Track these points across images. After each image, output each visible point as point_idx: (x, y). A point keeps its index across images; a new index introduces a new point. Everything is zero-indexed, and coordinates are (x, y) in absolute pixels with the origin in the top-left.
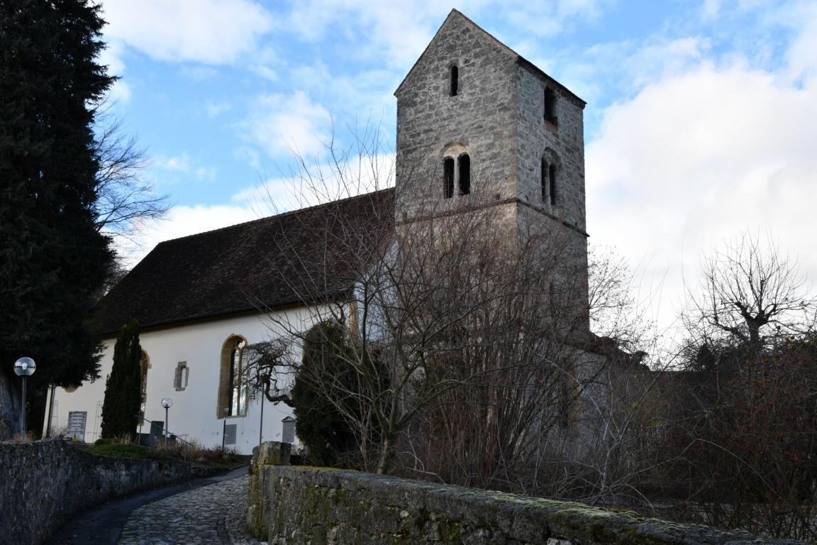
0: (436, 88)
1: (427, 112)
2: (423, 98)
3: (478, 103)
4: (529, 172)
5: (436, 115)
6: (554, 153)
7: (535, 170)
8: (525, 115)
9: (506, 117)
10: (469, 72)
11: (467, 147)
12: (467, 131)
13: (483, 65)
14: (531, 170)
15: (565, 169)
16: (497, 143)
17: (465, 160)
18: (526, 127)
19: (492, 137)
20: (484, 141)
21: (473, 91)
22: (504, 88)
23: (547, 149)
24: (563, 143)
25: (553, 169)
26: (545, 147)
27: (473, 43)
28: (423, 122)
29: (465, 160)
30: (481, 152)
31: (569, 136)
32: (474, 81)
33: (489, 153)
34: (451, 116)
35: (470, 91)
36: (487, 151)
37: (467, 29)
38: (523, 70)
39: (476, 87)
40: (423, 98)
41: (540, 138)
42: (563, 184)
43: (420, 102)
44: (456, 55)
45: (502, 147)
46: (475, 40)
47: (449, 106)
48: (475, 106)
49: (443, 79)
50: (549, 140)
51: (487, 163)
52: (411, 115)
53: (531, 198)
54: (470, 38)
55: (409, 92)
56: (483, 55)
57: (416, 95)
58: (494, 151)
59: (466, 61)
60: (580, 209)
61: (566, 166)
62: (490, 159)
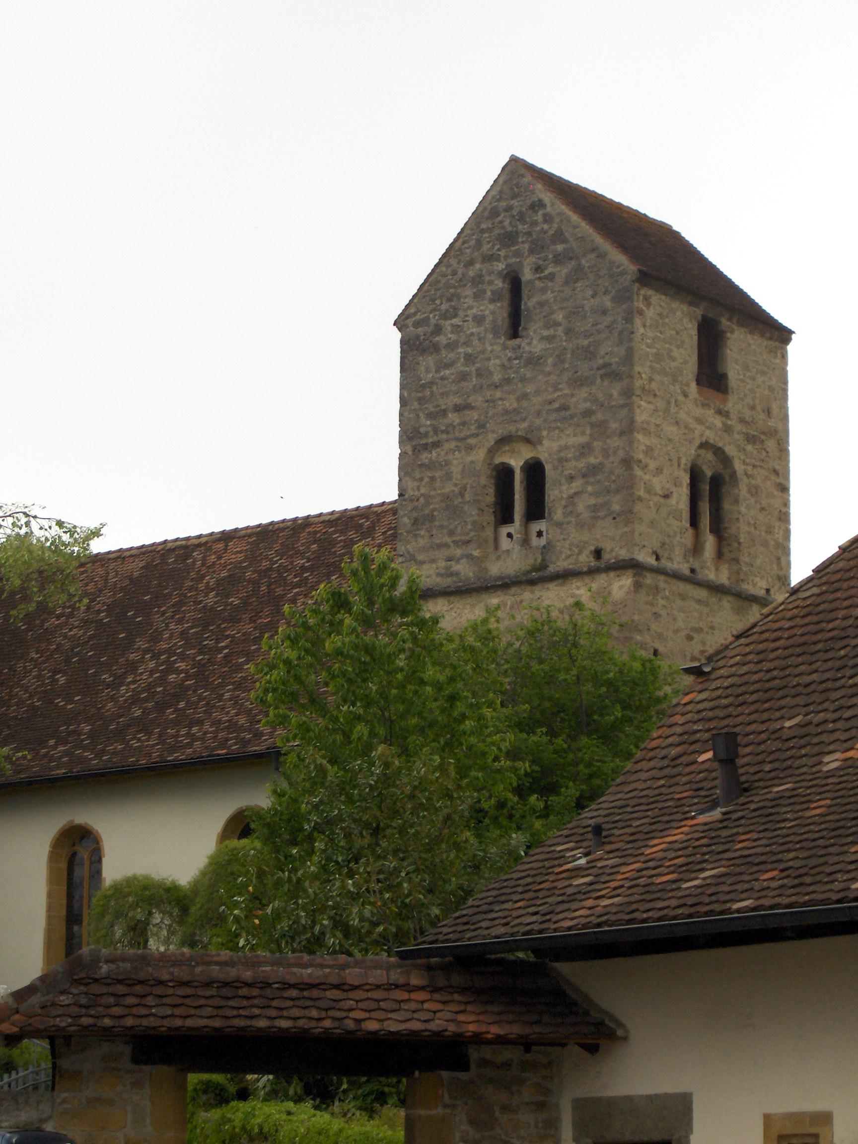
0: (479, 320)
1: (460, 367)
2: (453, 337)
3: (560, 359)
4: (662, 500)
5: (479, 375)
6: (718, 452)
7: (675, 494)
8: (654, 386)
9: (615, 393)
10: (543, 290)
11: (539, 447)
12: (539, 413)
13: (569, 281)
14: (666, 497)
15: (745, 478)
16: (598, 444)
17: (504, 515)
18: (656, 410)
19: (588, 432)
20: (573, 439)
21: (551, 332)
22: (610, 332)
23: (702, 446)
24: (739, 427)
25: (717, 483)
26: (697, 442)
27: (552, 232)
28: (453, 388)
29: (535, 472)
30: (567, 460)
31: (753, 408)
32: (552, 313)
33: (581, 464)
34: (508, 381)
35: (546, 333)
36: (577, 459)
37: (540, 200)
38: (650, 292)
39: (557, 324)
40: (453, 337)
41: (686, 427)
42: (743, 511)
43: (447, 346)
44: (518, 254)
45: (606, 453)
46: (556, 225)
47: (505, 361)
48: (555, 365)
49: (492, 301)
50: (709, 428)
51: (577, 484)
52: (427, 370)
53: (664, 554)
54: (545, 221)
55: (424, 322)
56: (571, 259)
57: (438, 330)
58: (592, 460)
59: (538, 269)
60: (779, 559)
61: (746, 474)
62: (584, 476)
